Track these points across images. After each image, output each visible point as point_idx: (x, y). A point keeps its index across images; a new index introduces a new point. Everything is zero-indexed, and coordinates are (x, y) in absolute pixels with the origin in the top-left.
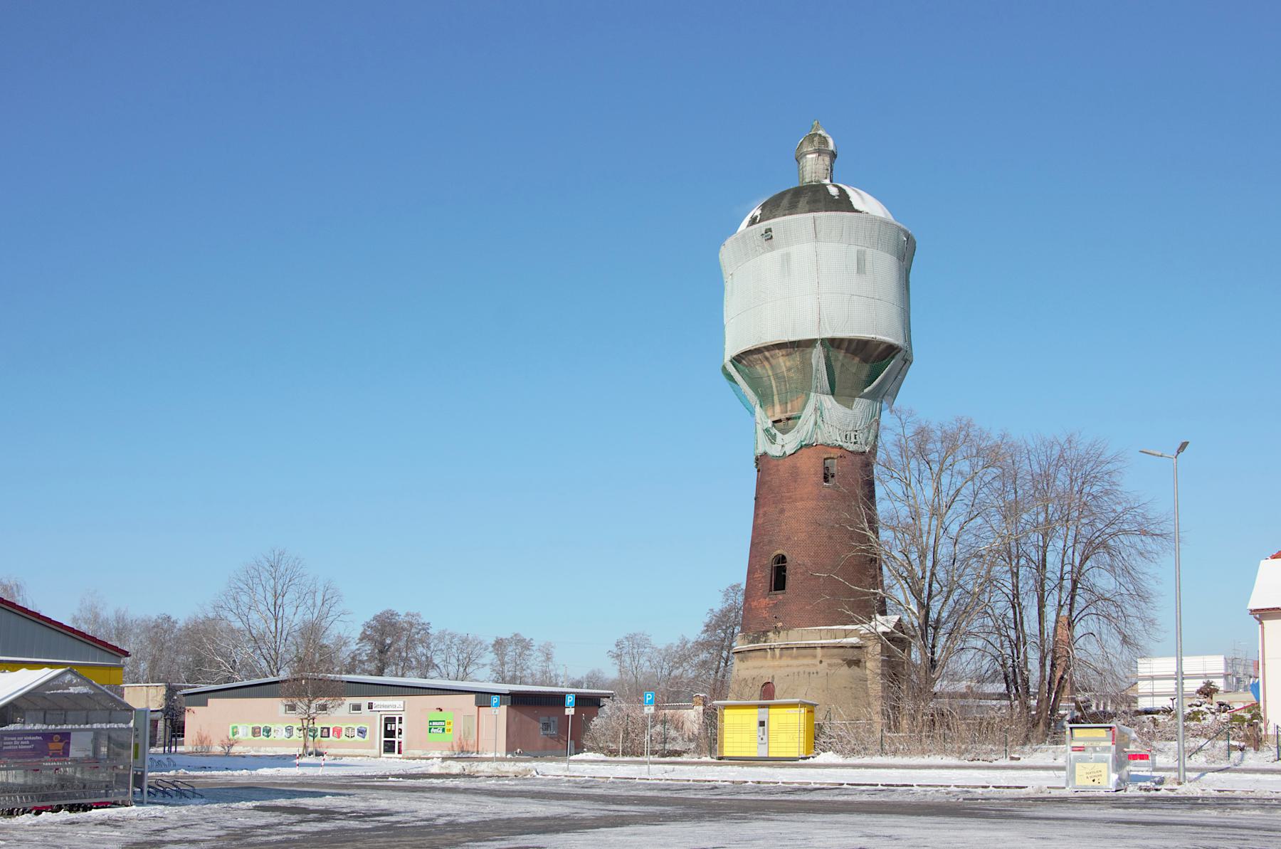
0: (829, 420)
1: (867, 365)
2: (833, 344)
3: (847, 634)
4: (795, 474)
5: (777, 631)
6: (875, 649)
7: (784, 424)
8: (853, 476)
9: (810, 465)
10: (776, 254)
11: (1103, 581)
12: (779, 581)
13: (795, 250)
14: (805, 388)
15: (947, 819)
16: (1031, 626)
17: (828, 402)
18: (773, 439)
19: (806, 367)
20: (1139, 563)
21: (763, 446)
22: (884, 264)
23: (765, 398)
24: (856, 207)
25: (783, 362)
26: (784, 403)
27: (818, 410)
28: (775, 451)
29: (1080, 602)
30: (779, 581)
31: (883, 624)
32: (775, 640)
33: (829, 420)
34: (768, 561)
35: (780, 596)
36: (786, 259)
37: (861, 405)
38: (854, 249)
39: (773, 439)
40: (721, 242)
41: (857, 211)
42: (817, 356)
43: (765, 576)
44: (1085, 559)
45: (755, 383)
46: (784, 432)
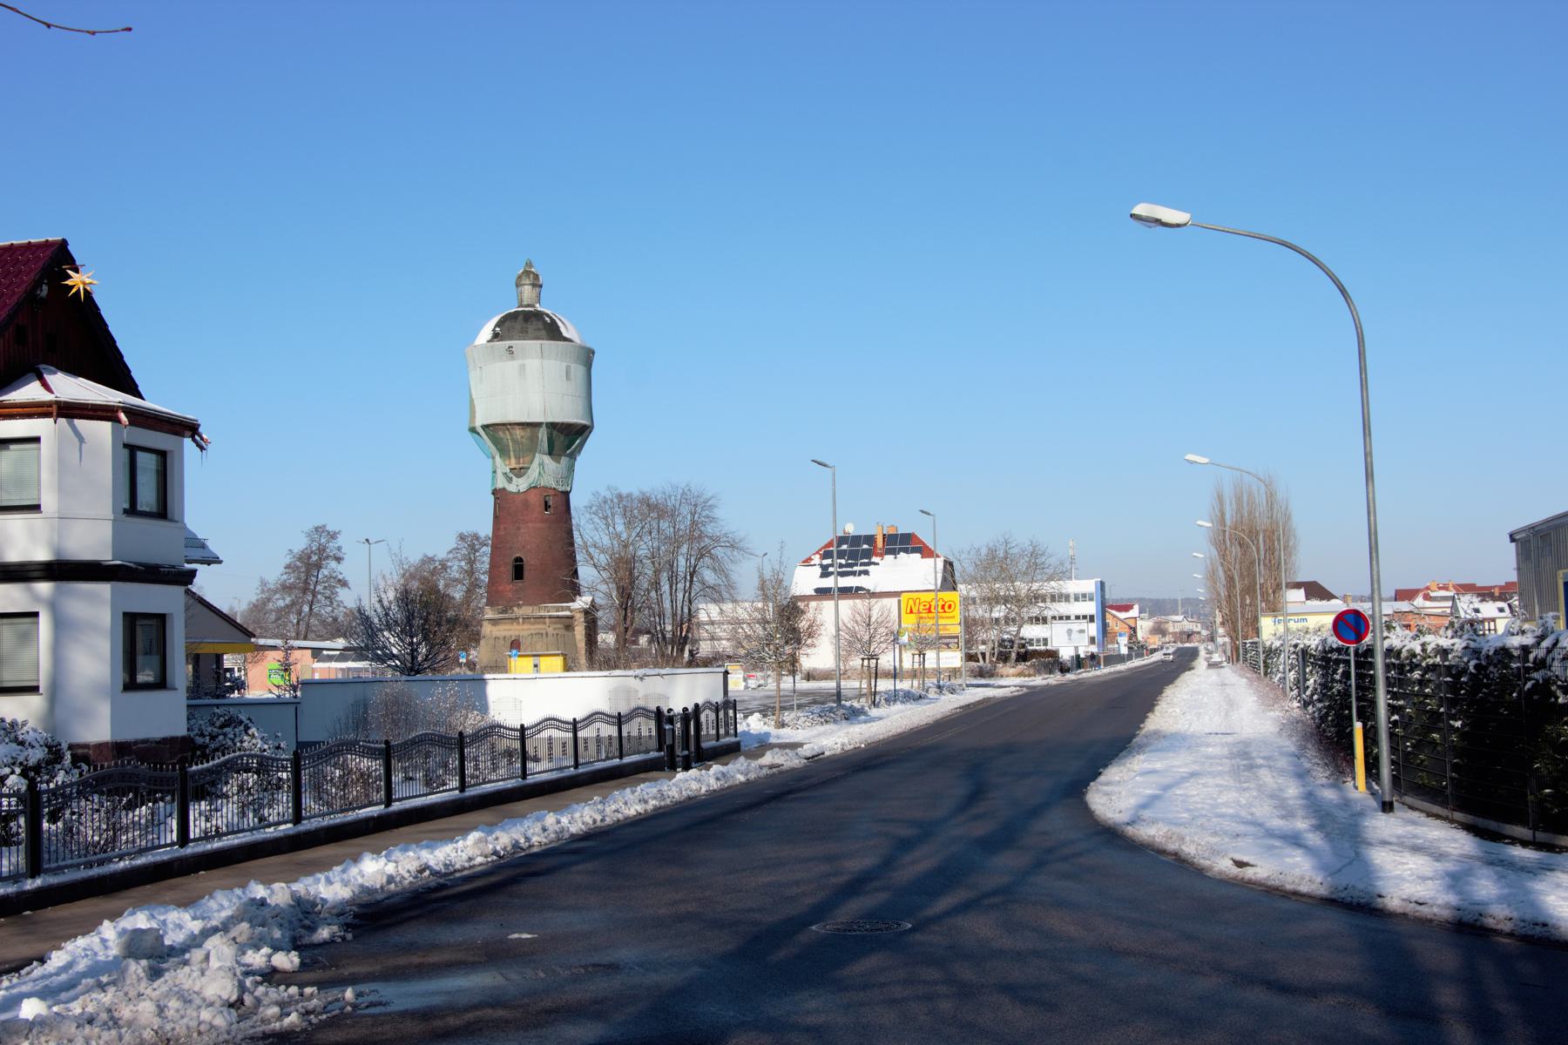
0: (543, 470)
1: (567, 438)
2: (552, 426)
3: (563, 609)
4: (526, 504)
5: (519, 606)
6: (580, 618)
7: (520, 472)
8: (558, 505)
9: (535, 500)
10: (515, 364)
11: (709, 576)
12: (519, 571)
13: (528, 362)
14: (532, 449)
15: (387, 833)
16: (667, 605)
17: (547, 459)
18: (510, 480)
19: (533, 439)
20: (729, 566)
21: (501, 483)
22: (577, 370)
23: (504, 452)
24: (565, 334)
25: (518, 432)
26: (518, 458)
27: (541, 464)
28: (512, 488)
29: (697, 586)
30: (519, 571)
31: (582, 602)
32: (518, 612)
33: (543, 470)
34: (510, 561)
35: (519, 583)
36: (523, 368)
37: (564, 460)
38: (564, 365)
39: (510, 480)
40: (1084, 794)
41: (566, 339)
42: (543, 434)
43: (507, 570)
44: (698, 560)
45: (496, 442)
46: (519, 476)
